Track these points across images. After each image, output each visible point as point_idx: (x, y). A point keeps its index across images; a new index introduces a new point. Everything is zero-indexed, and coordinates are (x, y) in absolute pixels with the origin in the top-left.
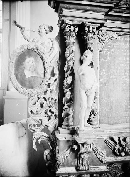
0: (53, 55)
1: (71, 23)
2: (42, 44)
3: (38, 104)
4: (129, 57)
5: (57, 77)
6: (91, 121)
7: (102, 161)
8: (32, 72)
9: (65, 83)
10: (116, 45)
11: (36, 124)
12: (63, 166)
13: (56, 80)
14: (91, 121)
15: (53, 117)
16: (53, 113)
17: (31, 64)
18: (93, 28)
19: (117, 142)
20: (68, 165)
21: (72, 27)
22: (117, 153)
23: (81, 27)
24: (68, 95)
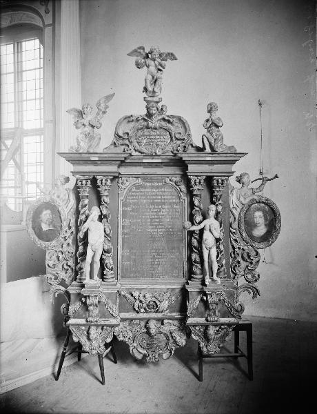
0: (69, 207)
1: (82, 178)
2: (58, 197)
3: (54, 257)
4: (4, 300)
5: (73, 229)
6: (105, 275)
7: (112, 315)
8: (49, 225)
9: (78, 238)
10: (141, 192)
11: (53, 278)
12: (74, 317)
13: (72, 232)
14: (105, 275)
15: (70, 271)
16: (70, 266)
17: (48, 216)
18: (106, 180)
19: (237, 218)
20: (79, 317)
21: (84, 182)
22: (137, 309)
23: (94, 181)
24: (81, 248)
